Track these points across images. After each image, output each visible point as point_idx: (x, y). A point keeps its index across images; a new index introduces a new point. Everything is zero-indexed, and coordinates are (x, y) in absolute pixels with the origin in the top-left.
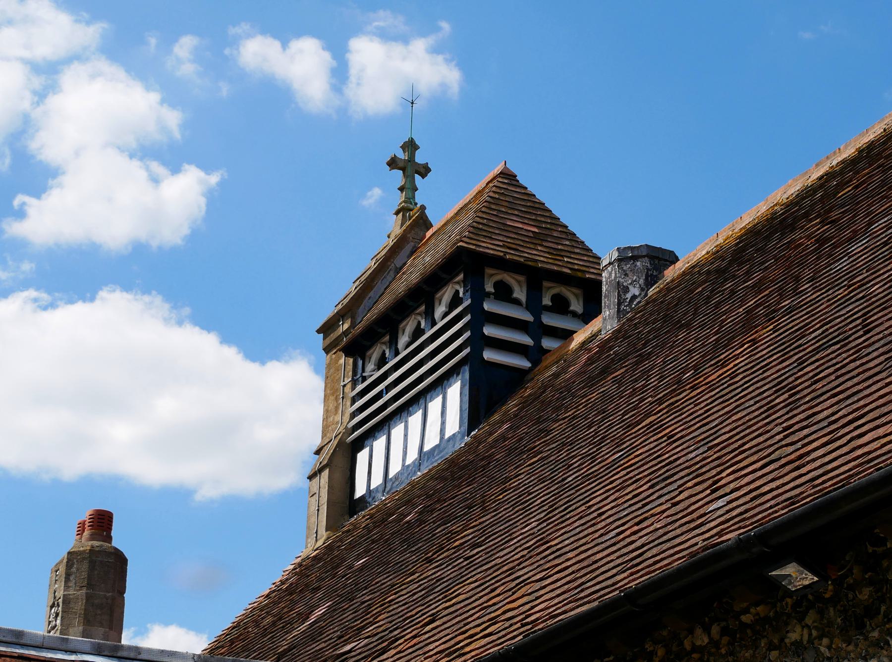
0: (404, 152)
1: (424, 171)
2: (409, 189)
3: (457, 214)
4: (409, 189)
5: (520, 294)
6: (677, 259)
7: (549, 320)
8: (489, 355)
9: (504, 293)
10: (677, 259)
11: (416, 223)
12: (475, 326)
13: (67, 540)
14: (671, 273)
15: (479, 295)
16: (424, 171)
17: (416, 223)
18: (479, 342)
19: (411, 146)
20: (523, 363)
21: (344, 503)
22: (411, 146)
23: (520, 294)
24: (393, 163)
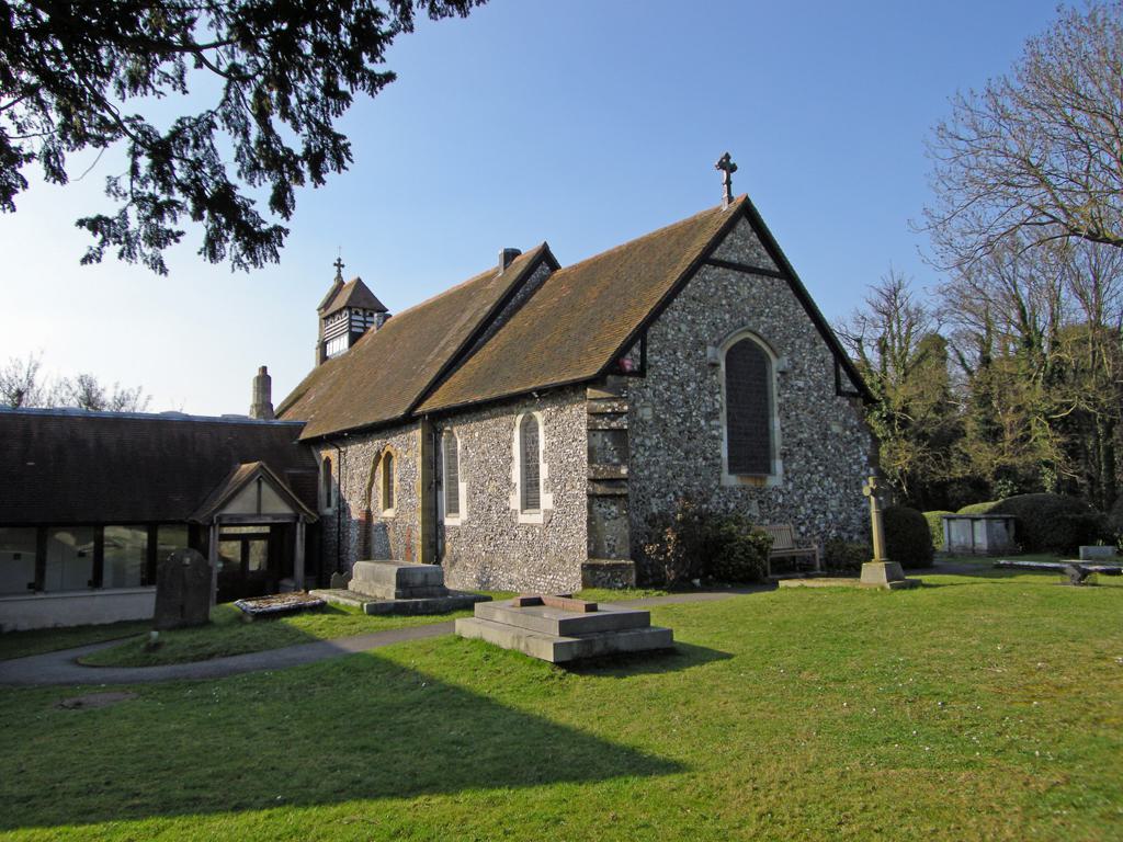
0: (95, 234)
1: (343, 266)
2: (339, 271)
3: (241, 653)
4: (339, 271)
5: (361, 313)
6: (561, 622)
7: (368, 319)
8: (353, 330)
9: (357, 313)
10: (561, 622)
11: (340, 284)
12: (350, 323)
13: (257, 373)
14: (388, 320)
15: (351, 315)
16: (343, 266)
17: (340, 284)
18: (351, 326)
19: (339, 260)
20: (362, 331)
21: (324, 358)
22: (339, 260)
23: (361, 313)
24: (335, 265)
